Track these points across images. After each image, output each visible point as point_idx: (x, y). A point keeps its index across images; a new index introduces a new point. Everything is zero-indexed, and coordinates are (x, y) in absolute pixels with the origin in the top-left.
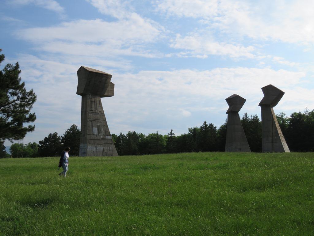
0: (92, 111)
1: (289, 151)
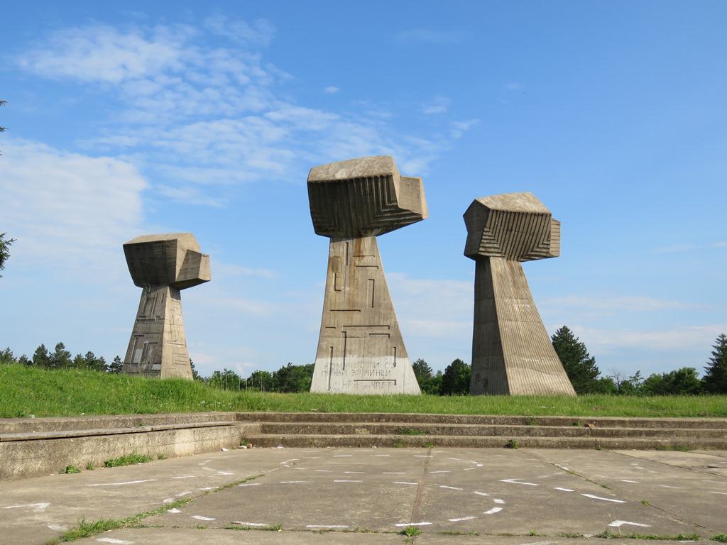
0: (143, 318)
1: (492, 261)
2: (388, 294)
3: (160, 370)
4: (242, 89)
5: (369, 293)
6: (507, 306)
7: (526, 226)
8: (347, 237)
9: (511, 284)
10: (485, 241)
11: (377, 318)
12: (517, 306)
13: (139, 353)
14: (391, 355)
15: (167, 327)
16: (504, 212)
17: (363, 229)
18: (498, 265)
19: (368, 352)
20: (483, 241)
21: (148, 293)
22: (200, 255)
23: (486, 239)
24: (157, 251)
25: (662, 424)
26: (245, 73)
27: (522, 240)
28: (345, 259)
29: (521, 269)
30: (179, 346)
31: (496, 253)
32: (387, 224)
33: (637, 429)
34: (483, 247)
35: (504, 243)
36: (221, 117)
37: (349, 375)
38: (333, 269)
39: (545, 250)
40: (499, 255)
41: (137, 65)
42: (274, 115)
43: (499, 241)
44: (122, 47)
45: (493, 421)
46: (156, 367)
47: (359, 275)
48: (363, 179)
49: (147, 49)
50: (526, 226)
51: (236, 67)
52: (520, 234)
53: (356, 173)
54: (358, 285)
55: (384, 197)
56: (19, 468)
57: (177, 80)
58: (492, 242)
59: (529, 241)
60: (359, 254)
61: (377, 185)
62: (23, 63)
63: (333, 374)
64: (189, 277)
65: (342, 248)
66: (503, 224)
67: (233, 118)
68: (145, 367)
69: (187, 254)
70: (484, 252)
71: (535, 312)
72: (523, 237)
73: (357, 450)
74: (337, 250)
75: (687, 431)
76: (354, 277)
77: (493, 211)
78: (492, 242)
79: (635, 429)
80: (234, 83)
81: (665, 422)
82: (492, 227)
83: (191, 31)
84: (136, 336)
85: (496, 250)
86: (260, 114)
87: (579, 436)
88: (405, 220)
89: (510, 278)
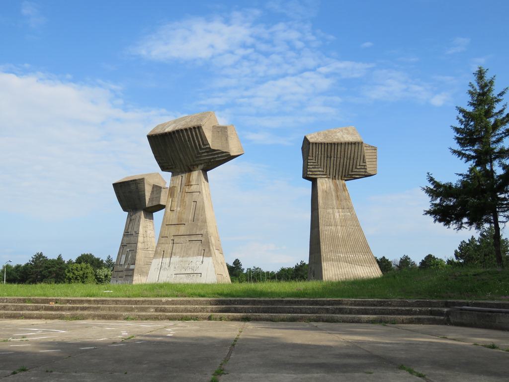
2: (204, 212)
3: (134, 269)
4: (299, 51)
5: (192, 211)
6: (330, 214)
7: (342, 153)
8: (182, 172)
9: (334, 198)
10: (311, 167)
11: (195, 229)
12: (338, 215)
13: (124, 257)
14: (201, 255)
15: (140, 239)
16: (321, 144)
17: (191, 165)
18: (324, 184)
20: (309, 167)
21: (131, 216)
22: (160, 188)
23: (311, 165)
24: (133, 187)
25: (116, 302)
26: (300, 40)
27: (341, 164)
28: (179, 188)
29: (344, 185)
31: (322, 175)
32: (207, 161)
33: (75, 305)
34: (310, 171)
35: (326, 167)
36: (284, 76)
37: (172, 271)
38: (171, 196)
39: (363, 170)
40: (325, 176)
41: (221, 44)
42: (323, 70)
43: (322, 165)
44: (210, 32)
45: (5, 301)
46: (132, 267)
47: (187, 198)
48: (182, 130)
49: (226, 30)
50: (342, 153)
51: (294, 35)
52: (338, 160)
53: (179, 126)
54: (185, 206)
55: (199, 142)
57: (250, 51)
58: (316, 167)
59: (348, 164)
60: (189, 184)
61: (192, 134)
62: (143, 52)
63: (162, 270)
64: (155, 203)
65: (180, 179)
66: (323, 153)
67: (293, 75)
68: (126, 267)
69: (153, 188)
70: (311, 175)
71: (354, 218)
72: (342, 161)
73: (49, 321)
74: (175, 182)
75: (109, 307)
76: (183, 200)
77: (313, 143)
78: (316, 167)
79: (73, 305)
80: (292, 48)
81: (118, 301)
82: (314, 156)
83: (257, 12)
84: (123, 246)
85: (321, 173)
86: (313, 70)
87: (36, 310)
89: (334, 193)
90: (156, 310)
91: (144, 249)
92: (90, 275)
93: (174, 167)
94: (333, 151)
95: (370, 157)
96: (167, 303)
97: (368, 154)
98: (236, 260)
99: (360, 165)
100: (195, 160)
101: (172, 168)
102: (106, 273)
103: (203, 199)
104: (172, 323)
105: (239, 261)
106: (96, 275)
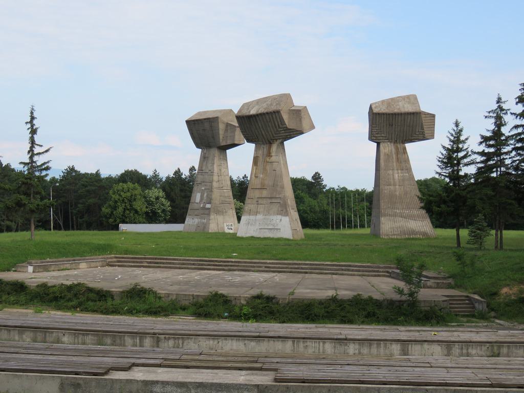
0: (202, 172)
9: (394, 160)
11: (275, 193)
15: (215, 178)
19: (268, 213)
24: (207, 125)
29: (405, 149)
30: (225, 191)
47: (268, 167)
53: (262, 110)
56: (37, 270)
64: (229, 142)
88: (294, 134)
90: (266, 267)
91: (219, 188)
92: (139, 197)
93: (257, 140)
94: (394, 119)
95: (429, 124)
96: (270, 263)
97: (427, 124)
98: (316, 173)
99: (418, 132)
100: (275, 135)
101: (255, 141)
102: (157, 194)
103: (281, 168)
104: (279, 275)
105: (319, 174)
106: (145, 197)
